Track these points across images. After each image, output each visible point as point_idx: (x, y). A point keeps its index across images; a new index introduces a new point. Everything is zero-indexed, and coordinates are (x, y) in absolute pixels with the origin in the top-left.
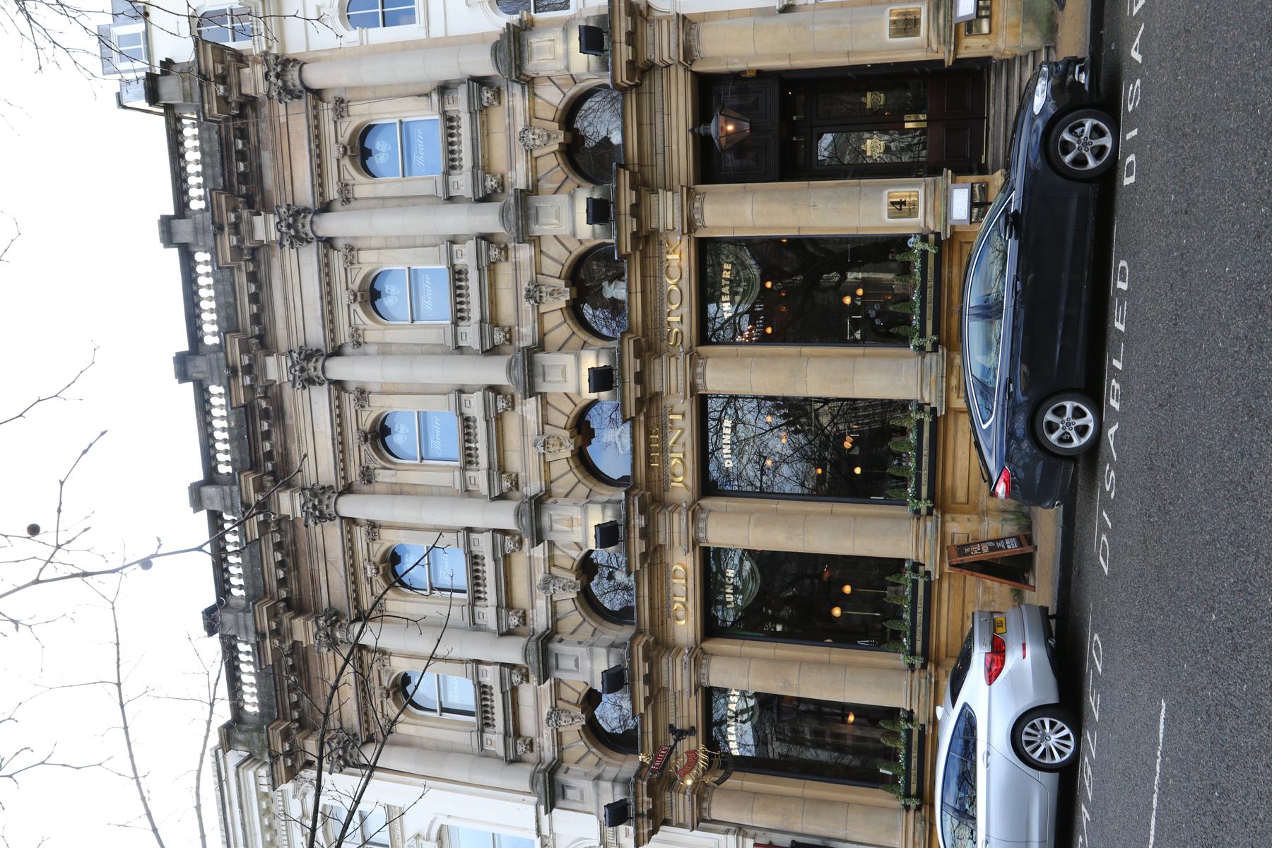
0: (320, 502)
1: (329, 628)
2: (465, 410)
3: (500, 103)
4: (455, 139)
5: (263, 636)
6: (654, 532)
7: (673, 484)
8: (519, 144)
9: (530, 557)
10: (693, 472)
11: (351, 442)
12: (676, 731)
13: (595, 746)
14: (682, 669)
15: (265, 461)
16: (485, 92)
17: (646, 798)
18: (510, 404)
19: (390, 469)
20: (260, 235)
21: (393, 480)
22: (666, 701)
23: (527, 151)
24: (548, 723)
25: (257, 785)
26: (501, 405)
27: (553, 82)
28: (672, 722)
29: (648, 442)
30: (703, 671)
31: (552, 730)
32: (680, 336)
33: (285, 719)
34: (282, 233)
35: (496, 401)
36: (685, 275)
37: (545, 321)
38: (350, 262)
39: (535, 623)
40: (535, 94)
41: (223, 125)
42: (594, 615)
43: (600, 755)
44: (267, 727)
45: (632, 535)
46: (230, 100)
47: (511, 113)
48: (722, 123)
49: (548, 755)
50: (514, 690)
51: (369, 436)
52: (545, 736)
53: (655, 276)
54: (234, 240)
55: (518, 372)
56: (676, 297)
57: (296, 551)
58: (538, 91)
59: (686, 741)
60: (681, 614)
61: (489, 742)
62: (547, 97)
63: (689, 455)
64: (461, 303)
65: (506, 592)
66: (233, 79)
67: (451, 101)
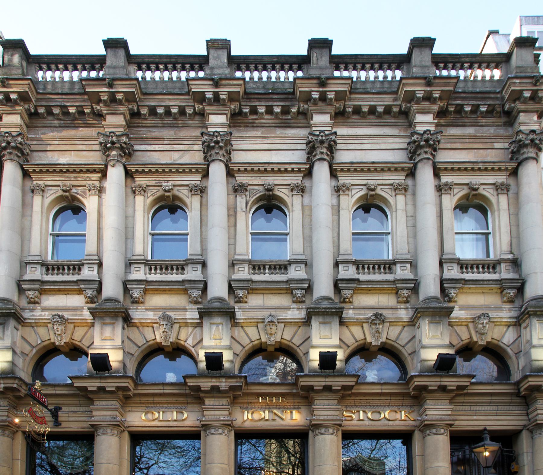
0: (221, 148)
1: (119, 146)
2: (293, 266)
3: (505, 302)
4: (481, 270)
5: (111, 86)
6: (214, 397)
7: (246, 412)
8: (478, 313)
9: (186, 309)
10: (255, 426)
11: (266, 178)
12: (57, 412)
13: (37, 352)
14: (111, 415)
15: (250, 106)
16: (514, 291)
18: (299, 299)
19: (246, 208)
20: (419, 118)
21: (238, 209)
22: (80, 405)
23: (473, 319)
24: (56, 315)
26: (299, 293)
27: (517, 339)
28: (64, 409)
29: (277, 395)
30: (109, 431)
31: (49, 319)
32: (349, 419)
33: (38, 100)
34: (422, 135)
35: (301, 289)
36: (391, 423)
37: (356, 327)
38: (397, 189)
39: (135, 310)
40: (509, 326)
41: (499, 96)
42: (142, 356)
43: (31, 355)
44: (30, 79)
45: (214, 380)
46: (517, 102)
47: (498, 309)
48: (492, 448)
49: (27, 315)
50: (80, 291)
51: (271, 193)
52: (43, 313)
53: (390, 402)
54: (420, 95)
55: (325, 304)
56: (376, 416)
57: (176, 127)
58: (511, 328)
59: (51, 419)
60: (150, 416)
61: (34, 269)
62: (507, 335)
63: (267, 423)
64: (369, 268)
65: (157, 290)
66: (532, 106)
67: (507, 268)
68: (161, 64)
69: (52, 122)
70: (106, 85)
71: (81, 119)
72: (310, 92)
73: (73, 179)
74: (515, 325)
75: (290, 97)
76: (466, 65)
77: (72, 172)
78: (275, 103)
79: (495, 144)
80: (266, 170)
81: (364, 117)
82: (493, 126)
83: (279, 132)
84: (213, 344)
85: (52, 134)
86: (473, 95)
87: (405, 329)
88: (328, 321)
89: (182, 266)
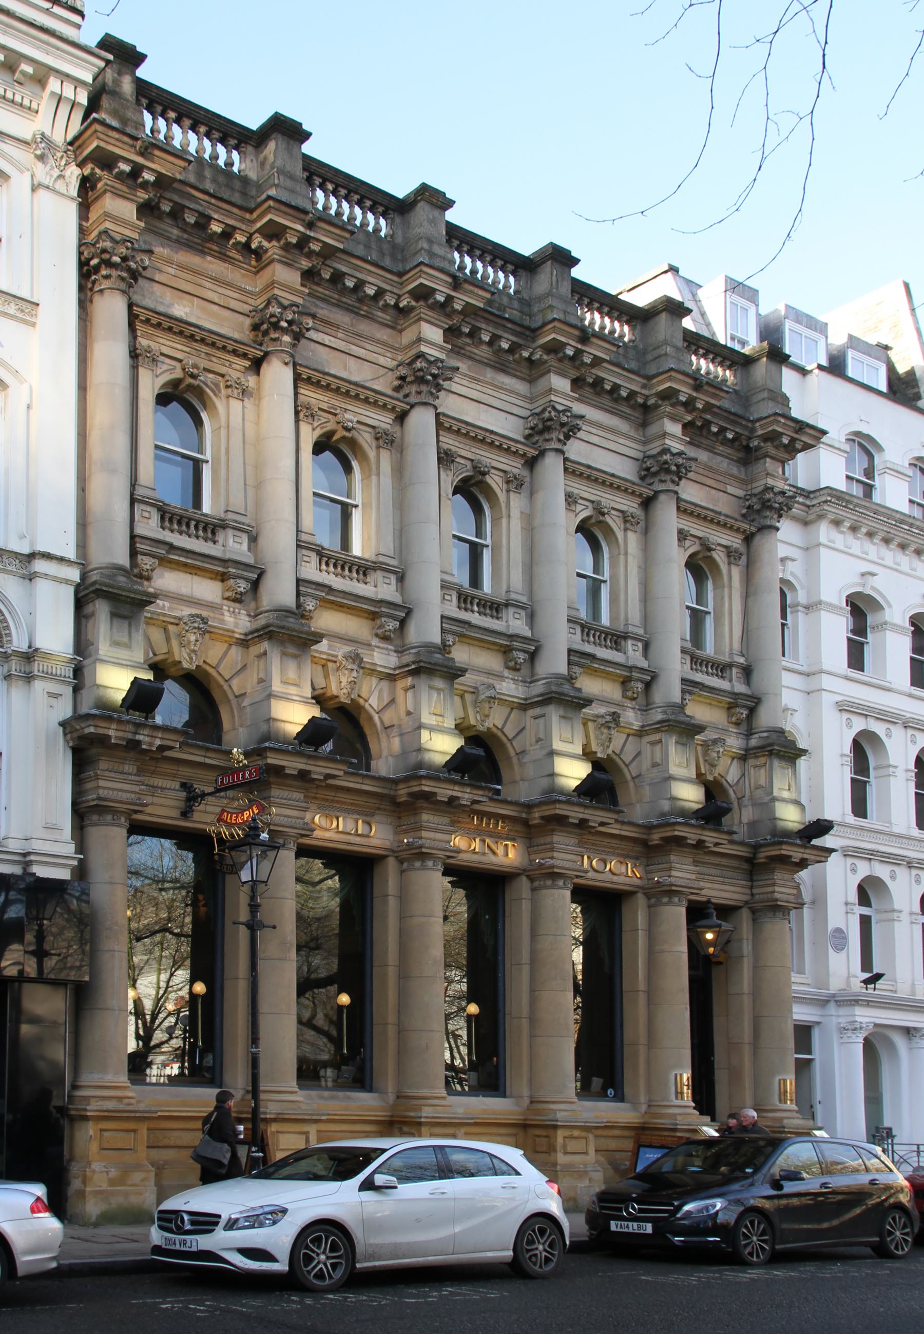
2: (511, 610)
5: (310, 225)
11: (478, 451)
17: (158, 742)
24: (198, 616)
25: (65, 77)
36: (615, 878)
40: (733, 759)
41: (750, 425)
45: (456, 788)
50: (223, 577)
57: (357, 314)
63: (475, 858)
68: (332, 182)
69: (170, 229)
70: (304, 221)
71: (218, 244)
72: (782, 434)
73: (203, 355)
74: (739, 758)
75: (528, 333)
76: (701, 351)
77: (207, 345)
78: (506, 335)
79: (728, 487)
80: (483, 441)
81: (598, 394)
82: (727, 458)
83: (490, 374)
84: (434, 723)
85: (161, 249)
86: (725, 414)
87: (630, 738)
88: (570, 715)
89: (367, 569)
